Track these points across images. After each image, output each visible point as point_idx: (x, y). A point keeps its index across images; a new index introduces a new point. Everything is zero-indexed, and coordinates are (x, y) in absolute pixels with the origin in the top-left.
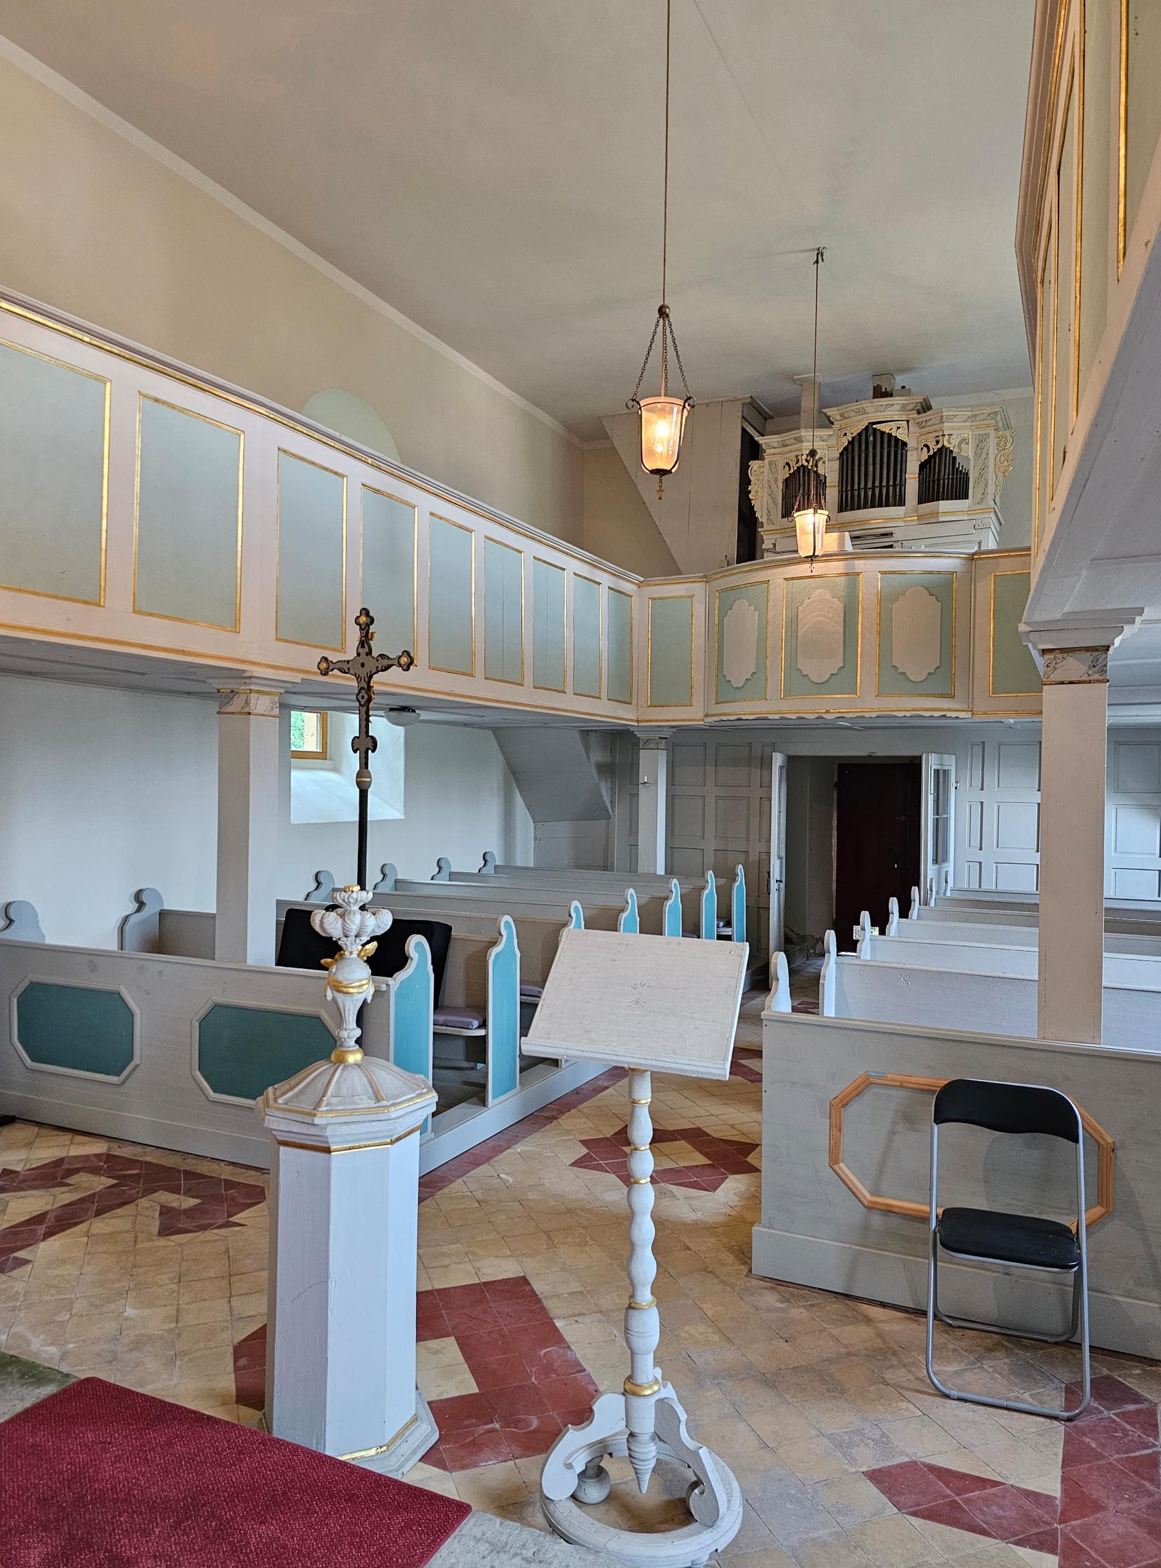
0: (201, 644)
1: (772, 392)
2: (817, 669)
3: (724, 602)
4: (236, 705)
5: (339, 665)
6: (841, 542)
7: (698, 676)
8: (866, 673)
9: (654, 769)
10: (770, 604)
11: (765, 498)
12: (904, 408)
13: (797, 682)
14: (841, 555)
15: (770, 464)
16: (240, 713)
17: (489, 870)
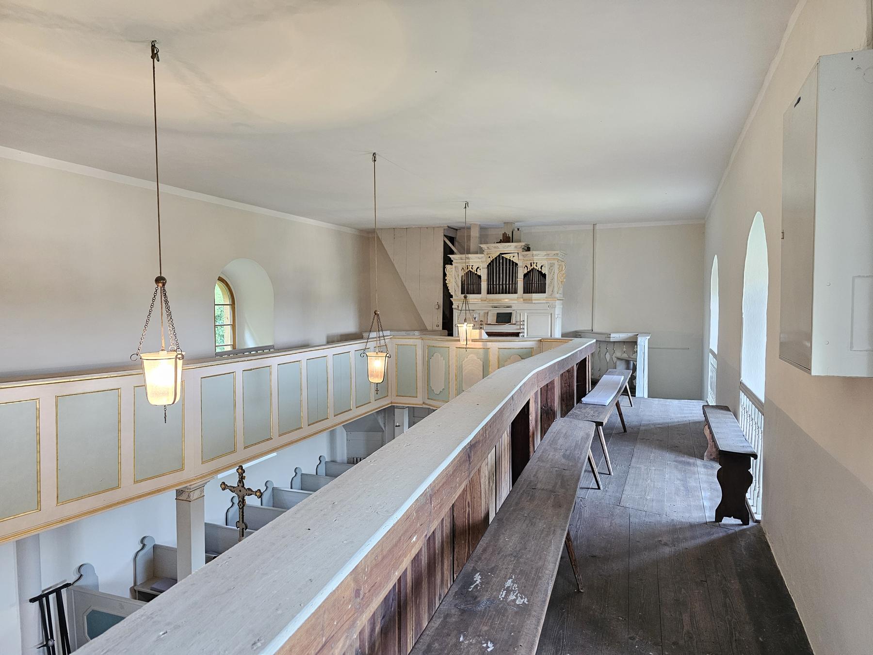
3: (430, 353)
6: (481, 334)
11: (454, 287)
12: (516, 247)
14: (480, 340)
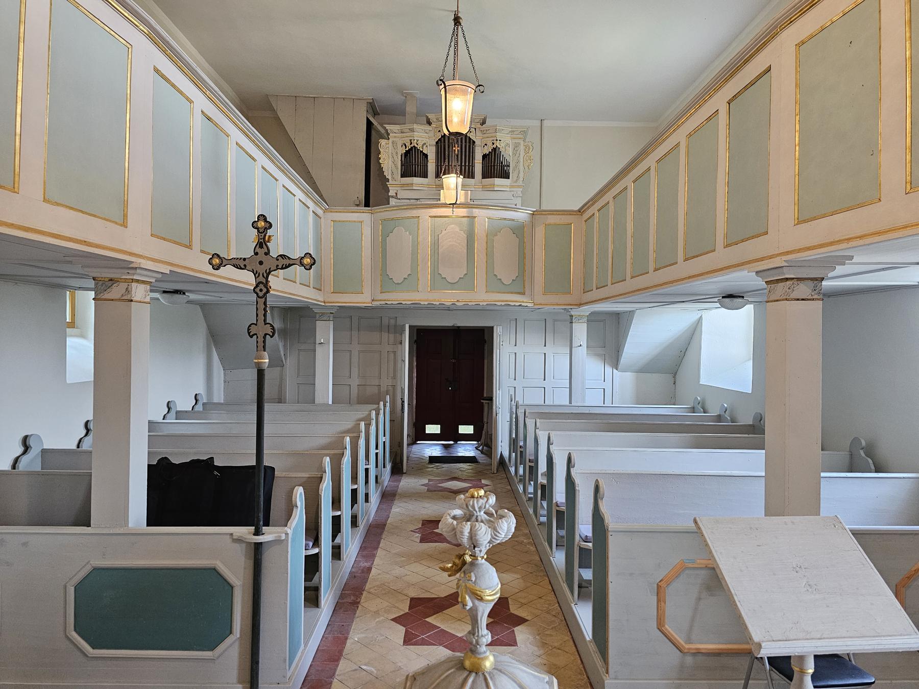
0: (99, 236)
1: (390, 97)
2: (452, 274)
4: (116, 292)
5: (234, 262)
7: (367, 274)
8: (480, 279)
9: (325, 332)
10: (420, 231)
13: (438, 282)
15: (393, 142)
16: (119, 300)
17: (199, 407)
